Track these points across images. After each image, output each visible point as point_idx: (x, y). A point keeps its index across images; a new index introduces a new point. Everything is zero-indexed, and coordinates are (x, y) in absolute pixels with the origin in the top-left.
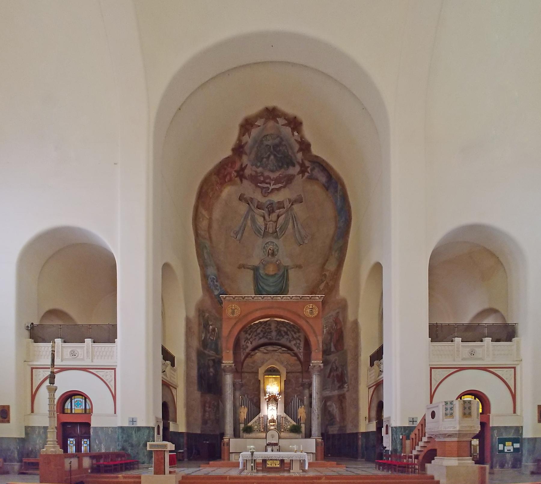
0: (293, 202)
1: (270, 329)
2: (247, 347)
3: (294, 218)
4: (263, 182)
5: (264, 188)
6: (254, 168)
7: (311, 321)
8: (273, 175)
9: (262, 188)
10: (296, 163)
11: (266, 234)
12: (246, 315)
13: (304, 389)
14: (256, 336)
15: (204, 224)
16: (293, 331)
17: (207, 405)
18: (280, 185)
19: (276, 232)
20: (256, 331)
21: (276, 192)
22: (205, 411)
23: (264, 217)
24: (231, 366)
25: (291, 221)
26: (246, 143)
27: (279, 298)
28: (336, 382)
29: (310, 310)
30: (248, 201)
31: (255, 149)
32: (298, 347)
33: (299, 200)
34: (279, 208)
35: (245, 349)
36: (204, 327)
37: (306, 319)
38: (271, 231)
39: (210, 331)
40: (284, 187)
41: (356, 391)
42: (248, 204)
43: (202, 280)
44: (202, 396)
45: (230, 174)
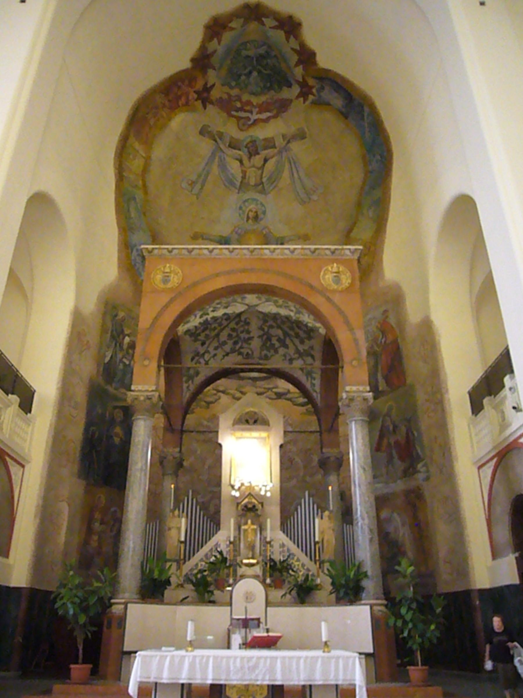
0: (289, 139)
1: (248, 332)
2: (197, 374)
3: (293, 163)
4: (241, 109)
5: (242, 118)
6: (226, 89)
7: (336, 298)
8: (255, 100)
9: (239, 118)
10: (293, 82)
11: (243, 186)
12: (195, 284)
13: (326, 474)
14: (216, 348)
15: (136, 164)
16: (297, 336)
17: (97, 515)
18: (268, 114)
19: (262, 183)
20: (217, 335)
21: (261, 124)
22: (90, 531)
23: (241, 161)
24: (149, 398)
25: (287, 166)
26: (215, 51)
27: (267, 252)
28: (396, 460)
29: (333, 277)
30: (216, 137)
31: (229, 62)
32: (309, 374)
33: (301, 136)
34: (266, 148)
35: (191, 378)
36: (113, 337)
37: (323, 292)
38: (252, 182)
39: (125, 347)
40: (275, 117)
41: (449, 475)
42: (215, 140)
43: (119, 251)
44: (87, 492)
45: (187, 94)
